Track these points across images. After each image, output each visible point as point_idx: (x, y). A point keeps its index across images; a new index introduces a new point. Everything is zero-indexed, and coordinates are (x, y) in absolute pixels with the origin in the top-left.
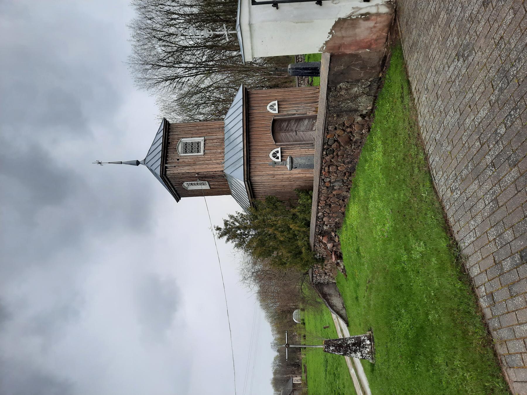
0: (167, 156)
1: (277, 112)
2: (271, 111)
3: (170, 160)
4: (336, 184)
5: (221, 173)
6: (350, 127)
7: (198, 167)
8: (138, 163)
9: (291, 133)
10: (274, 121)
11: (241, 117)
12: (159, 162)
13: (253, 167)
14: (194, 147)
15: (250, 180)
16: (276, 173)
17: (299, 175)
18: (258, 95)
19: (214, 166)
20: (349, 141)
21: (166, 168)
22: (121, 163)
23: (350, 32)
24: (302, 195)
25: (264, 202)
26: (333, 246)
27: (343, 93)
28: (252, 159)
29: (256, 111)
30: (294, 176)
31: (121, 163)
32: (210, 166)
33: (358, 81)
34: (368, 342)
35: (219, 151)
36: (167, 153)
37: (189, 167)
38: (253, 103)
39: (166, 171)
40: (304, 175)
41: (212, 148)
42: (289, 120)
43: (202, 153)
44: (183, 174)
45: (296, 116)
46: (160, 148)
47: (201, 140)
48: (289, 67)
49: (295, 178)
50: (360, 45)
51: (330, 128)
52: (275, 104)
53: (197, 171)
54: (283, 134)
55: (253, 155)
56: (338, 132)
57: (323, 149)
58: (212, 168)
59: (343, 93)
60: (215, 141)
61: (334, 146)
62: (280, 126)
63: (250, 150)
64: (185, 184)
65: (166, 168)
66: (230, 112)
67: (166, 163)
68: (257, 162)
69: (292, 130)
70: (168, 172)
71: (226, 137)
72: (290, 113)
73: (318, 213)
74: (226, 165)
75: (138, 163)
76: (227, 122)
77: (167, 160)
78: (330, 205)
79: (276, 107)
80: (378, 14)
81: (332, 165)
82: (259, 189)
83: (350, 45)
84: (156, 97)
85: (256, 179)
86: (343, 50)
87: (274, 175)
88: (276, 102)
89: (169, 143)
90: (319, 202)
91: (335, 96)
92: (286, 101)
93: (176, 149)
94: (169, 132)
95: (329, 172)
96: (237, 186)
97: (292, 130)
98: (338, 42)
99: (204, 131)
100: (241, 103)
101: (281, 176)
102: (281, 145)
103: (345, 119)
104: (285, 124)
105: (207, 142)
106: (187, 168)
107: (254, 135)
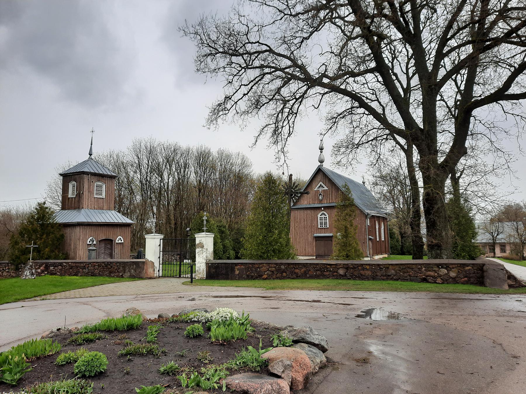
0: (95, 176)
1: (117, 242)
2: (118, 239)
3: (92, 177)
4: (87, 270)
5: (81, 206)
6: (118, 272)
7: (87, 193)
8: (90, 155)
9: (103, 250)
10: (112, 241)
11: (116, 221)
12: (92, 171)
13: (86, 227)
14: (99, 193)
15: (77, 225)
16: (81, 241)
17: (78, 254)
18: (128, 232)
19: (87, 203)
20: (111, 272)
21: (88, 175)
22: (91, 144)
23: (150, 267)
24: (64, 256)
25: (61, 233)
26: (39, 273)
27: (132, 267)
28: (91, 227)
29: (118, 230)
30: (78, 252)
31: (91, 144)
32: (87, 201)
33: (135, 271)
34: (33, 278)
35: (96, 207)
36: (97, 176)
37: (87, 188)
38: (123, 228)
39: (86, 174)
40: (77, 257)
41: (98, 202)
42: (111, 249)
43: (95, 196)
44: (83, 184)
45: (114, 253)
46: (101, 172)
47: (104, 196)
48: (142, 249)
49: (76, 252)
50: (147, 270)
51: (118, 264)
52: (121, 241)
53: (84, 193)
54: (103, 245)
55: (93, 227)
56: (116, 267)
57: (108, 262)
58: (85, 201)
59: (132, 267)
60: (102, 204)
61: (109, 267)
62: (108, 244)
63: (96, 226)
64: (74, 183)
65: (88, 175)
66: (118, 214)
67: (91, 175)
68: (88, 230)
69: (105, 250)
70: (85, 175)
71: (104, 211)
72: (116, 249)
73: (65, 263)
74: (87, 210)
75: (90, 155)
76: (113, 212)
77: (93, 175)
78: (71, 269)
79: (120, 242)
80: (154, 274)
81: (99, 267)
82: (68, 230)
83: (147, 267)
84: (127, 152)
85: (78, 229)
86: (146, 265)
87: (79, 239)
88: (123, 242)
89: (103, 177)
90: (74, 263)
91: (131, 264)
92: (123, 247)
93: (99, 181)
94: (110, 177)
95: (95, 266)
96: (72, 217)
97: (105, 250)
98: (148, 263)
99: (109, 198)
100: (124, 222)
101: (78, 244)
102: (97, 243)
103: (121, 269)
104: (109, 246)
105: (102, 200)
106: (87, 187)
107: (104, 229)
